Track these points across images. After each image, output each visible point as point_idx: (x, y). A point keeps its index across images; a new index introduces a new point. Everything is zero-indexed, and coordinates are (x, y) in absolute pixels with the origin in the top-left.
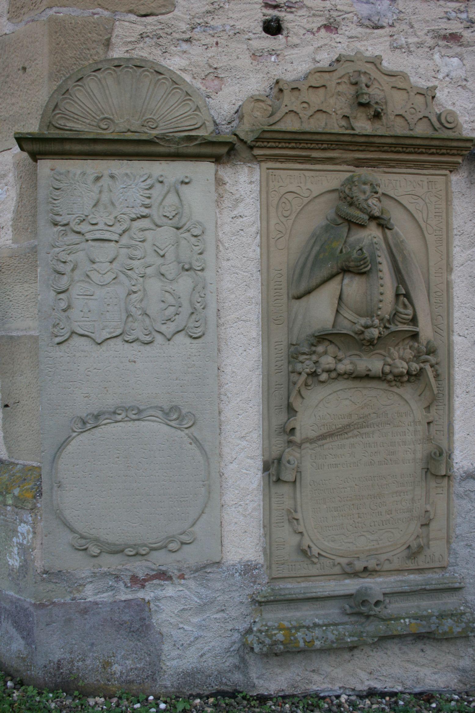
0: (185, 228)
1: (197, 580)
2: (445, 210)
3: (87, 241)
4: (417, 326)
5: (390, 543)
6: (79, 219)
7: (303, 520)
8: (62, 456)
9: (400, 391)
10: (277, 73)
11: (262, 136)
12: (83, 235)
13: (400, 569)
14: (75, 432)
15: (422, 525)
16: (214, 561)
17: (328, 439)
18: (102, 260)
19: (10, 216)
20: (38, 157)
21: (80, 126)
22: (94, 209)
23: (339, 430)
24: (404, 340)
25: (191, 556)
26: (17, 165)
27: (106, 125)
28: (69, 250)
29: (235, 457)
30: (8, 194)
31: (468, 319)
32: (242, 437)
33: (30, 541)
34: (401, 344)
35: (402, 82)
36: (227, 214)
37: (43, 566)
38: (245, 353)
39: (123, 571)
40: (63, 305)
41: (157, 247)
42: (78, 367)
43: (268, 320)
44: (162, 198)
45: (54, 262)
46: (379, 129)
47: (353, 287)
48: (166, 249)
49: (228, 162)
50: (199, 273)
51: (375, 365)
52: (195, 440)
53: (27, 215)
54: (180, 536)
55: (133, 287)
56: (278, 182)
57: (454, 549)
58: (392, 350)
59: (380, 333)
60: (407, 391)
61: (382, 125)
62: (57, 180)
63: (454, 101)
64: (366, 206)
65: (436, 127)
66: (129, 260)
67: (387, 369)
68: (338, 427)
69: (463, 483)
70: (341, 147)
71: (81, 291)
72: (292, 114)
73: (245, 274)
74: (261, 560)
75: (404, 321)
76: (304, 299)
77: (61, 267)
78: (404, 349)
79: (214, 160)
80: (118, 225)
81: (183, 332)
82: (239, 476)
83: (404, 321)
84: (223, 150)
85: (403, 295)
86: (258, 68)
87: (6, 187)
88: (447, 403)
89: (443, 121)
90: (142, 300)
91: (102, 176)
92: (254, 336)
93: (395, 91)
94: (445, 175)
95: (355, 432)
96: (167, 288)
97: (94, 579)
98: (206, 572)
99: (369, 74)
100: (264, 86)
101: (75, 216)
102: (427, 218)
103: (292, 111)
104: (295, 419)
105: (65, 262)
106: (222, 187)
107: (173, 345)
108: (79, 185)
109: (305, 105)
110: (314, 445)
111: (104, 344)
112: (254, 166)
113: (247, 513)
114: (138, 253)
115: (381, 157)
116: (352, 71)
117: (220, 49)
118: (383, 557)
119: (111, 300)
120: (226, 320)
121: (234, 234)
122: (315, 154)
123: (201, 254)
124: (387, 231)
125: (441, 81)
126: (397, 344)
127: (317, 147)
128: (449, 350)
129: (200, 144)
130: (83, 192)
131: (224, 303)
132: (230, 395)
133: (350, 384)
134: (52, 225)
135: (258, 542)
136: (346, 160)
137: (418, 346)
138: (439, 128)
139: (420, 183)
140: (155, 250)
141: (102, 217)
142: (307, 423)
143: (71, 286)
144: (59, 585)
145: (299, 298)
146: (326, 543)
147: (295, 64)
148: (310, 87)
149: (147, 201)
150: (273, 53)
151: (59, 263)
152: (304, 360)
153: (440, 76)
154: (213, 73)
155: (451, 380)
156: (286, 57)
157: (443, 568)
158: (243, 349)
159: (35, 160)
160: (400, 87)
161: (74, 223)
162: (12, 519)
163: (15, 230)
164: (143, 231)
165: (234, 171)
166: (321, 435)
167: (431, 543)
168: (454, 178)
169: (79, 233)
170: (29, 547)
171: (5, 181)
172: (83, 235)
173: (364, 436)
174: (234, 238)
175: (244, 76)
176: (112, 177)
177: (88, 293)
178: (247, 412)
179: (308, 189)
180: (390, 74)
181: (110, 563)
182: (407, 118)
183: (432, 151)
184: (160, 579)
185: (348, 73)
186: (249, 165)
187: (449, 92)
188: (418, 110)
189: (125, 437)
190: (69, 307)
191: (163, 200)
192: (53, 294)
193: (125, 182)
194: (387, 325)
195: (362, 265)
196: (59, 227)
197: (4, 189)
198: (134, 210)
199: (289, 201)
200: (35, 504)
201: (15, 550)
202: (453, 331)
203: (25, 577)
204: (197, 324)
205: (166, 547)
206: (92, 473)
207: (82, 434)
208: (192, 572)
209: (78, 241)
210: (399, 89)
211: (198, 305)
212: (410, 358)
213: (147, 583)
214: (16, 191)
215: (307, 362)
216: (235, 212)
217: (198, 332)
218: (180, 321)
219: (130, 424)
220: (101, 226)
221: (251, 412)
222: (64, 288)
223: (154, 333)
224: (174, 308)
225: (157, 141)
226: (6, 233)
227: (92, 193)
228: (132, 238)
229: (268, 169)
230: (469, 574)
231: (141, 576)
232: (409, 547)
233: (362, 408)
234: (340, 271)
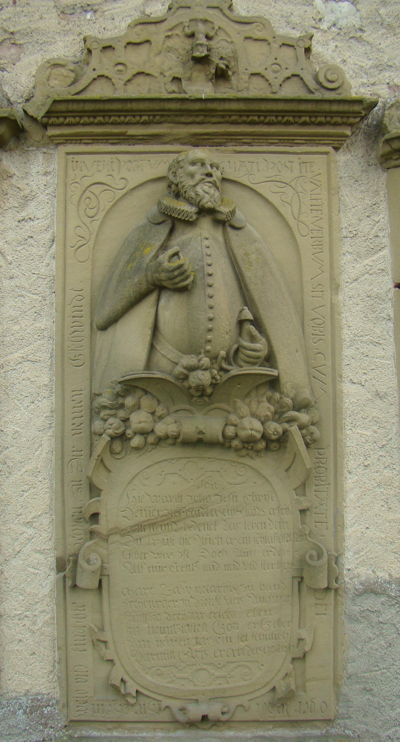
2: (326, 203)
4: (276, 368)
5: (245, 683)
7: (114, 642)
9: (257, 463)
10: (90, 31)
11: (53, 109)
13: (261, 719)
15: (294, 659)
17: (147, 531)
23: (164, 518)
24: (257, 387)
29: (18, 549)
31: (366, 358)
32: (28, 523)
34: (253, 394)
35: (260, 31)
38: (32, 406)
43: (63, 359)
46: (224, 91)
47: (171, 310)
49: (16, 148)
51: (211, 425)
56: (81, 170)
57: (345, 695)
58: (239, 403)
59: (213, 378)
60: (266, 464)
61: (230, 88)
63: (345, 58)
64: (193, 194)
65: (311, 89)
67: (230, 431)
68: (161, 513)
69: (359, 600)
70: (169, 119)
72: (103, 80)
73: (35, 297)
74: (57, 693)
75: (252, 360)
76: (110, 330)
78: (259, 402)
82: (25, 577)
83: (252, 360)
85: (252, 323)
86: (67, 28)
88: (332, 482)
89: (322, 79)
92: (45, 383)
93: (250, 44)
94: (327, 153)
95: (189, 522)
99: (212, 23)
100: (73, 50)
102: (299, 214)
103: (102, 76)
104: (99, 501)
106: (7, 181)
109: (120, 67)
110: (128, 538)
112: (51, 152)
113: (37, 628)
115: (228, 130)
116: (188, 20)
117: (18, 9)
118: (233, 703)
121: (20, 243)
122: (132, 131)
124: (231, 233)
125: (325, 32)
126: (248, 395)
127: (134, 120)
128: (335, 404)
131: (5, 336)
132: (11, 464)
133: (178, 452)
135: (52, 669)
136: (177, 137)
137: (281, 398)
138: (316, 90)
139: (289, 165)
142: (117, 506)
145: (104, 328)
146: (149, 677)
147: (117, 19)
148: (129, 44)
150: (89, 8)
152: (106, 417)
153: (324, 26)
154: (10, 39)
155: (339, 448)
156: (106, 13)
157: (328, 721)
160: (257, 37)
166: (138, 525)
167: (308, 684)
168: (342, 158)
173: (202, 528)
174: (20, 248)
175: (48, 40)
178: (35, 488)
179: (123, 178)
180: (242, 20)
182: (268, 78)
183: (303, 119)
185: (182, 23)
186: (45, 150)
187: (336, 46)
188: (284, 67)
194: (225, 366)
195: (176, 277)
199: (95, 195)
202: (341, 376)
210: (256, 40)
212: (266, 416)
215: (111, 420)
216: (24, 214)
221: (40, 488)
229: (68, 154)
230: (367, 731)
232: (274, 689)
233: (198, 487)
234: (152, 287)
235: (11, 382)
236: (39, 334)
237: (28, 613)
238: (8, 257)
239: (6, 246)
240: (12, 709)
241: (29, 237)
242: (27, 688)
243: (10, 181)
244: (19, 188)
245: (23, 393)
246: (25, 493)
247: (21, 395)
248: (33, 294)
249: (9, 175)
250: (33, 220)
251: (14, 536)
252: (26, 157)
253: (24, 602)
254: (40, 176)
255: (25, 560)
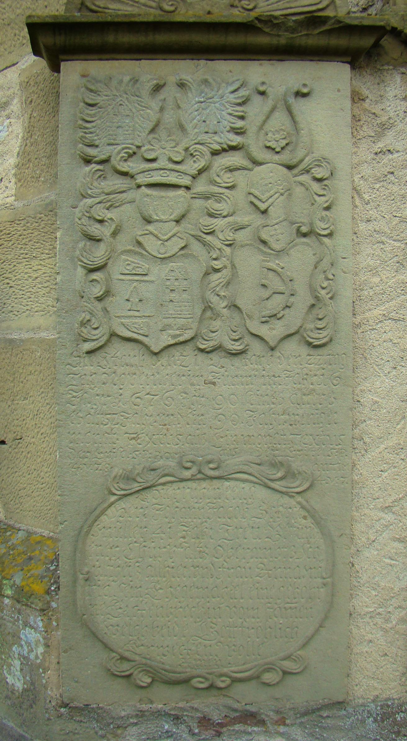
0: (301, 167)
1: (306, 727)
3: (139, 186)
6: (125, 153)
8: (92, 532)
12: (132, 177)
14: (115, 494)
16: (335, 699)
18: (163, 217)
19: (12, 161)
20: (61, 57)
21: (130, 9)
22: (152, 136)
25: (299, 692)
26: (25, 85)
27: (172, 5)
28: (109, 201)
29: (373, 538)
30: (10, 130)
32: (386, 507)
33: (41, 657)
36: (367, 147)
37: (61, 696)
38: (394, 372)
39: (188, 711)
40: (98, 291)
41: (256, 197)
42: (121, 391)
44: (264, 118)
45: (85, 221)
48: (271, 200)
49: (367, 66)
50: (326, 240)
52: (311, 513)
53: (38, 159)
54: (282, 662)
55: (215, 262)
62: (91, 91)
66: (207, 217)
71: (128, 267)
73: (396, 244)
77: (95, 230)
79: (349, 59)
80: (190, 161)
81: (296, 338)
84: (367, 42)
87: (8, 121)
90: (228, 283)
91: (165, 84)
96: (272, 265)
97: (140, 719)
98: (321, 716)
101: (119, 148)
105: (101, 222)
107: (279, 357)
108: (127, 98)
111: (163, 354)
113: (390, 625)
114: (223, 207)
119: (176, 283)
120: (365, 318)
121: (378, 180)
123: (328, 208)
129: (330, 32)
130: (134, 110)
131: (362, 290)
132: (367, 440)
134: (82, 162)
140: (252, 203)
141: (164, 149)
143: (111, 260)
144: (85, 725)
149: (240, 124)
151: (92, 222)
158: (391, 364)
159: (55, 68)
161: (118, 158)
162: (11, 617)
163: (20, 181)
164: (231, 171)
165: (377, 80)
169: (125, 174)
170: (39, 666)
171: (6, 112)
172: (132, 177)
176: (182, 85)
177: (140, 271)
178: (395, 467)
181: (166, 699)
184: (245, 723)
189: (196, 505)
190: (107, 293)
191: (265, 122)
192: (80, 271)
193: (202, 92)
196: (93, 165)
197: (5, 124)
198: (216, 138)
200: (48, 603)
201: (17, 663)
203: (31, 706)
204: (320, 324)
205: (258, 677)
206: (140, 559)
207: (125, 499)
208: (298, 715)
209: (124, 187)
211: (323, 292)
213: (225, 729)
214: (23, 125)
216: (380, 145)
217: (322, 337)
218: (294, 319)
219: (204, 484)
220: (162, 163)
222: (99, 262)
223: (248, 339)
224: (281, 296)
225: (259, 25)
226: (7, 187)
227: (149, 111)
228: (213, 183)
231: (216, 717)
235: (369, 344)
236: (402, 288)
237: (381, 610)
238: (364, 195)
239: (361, 182)
240: (360, 717)
241: (388, 172)
242: (376, 693)
243: (361, 105)
244: (374, 114)
245: (383, 357)
246: (383, 473)
247: (382, 359)
248: (394, 240)
249: (361, 98)
250: (392, 153)
251: (369, 523)
252: (380, 77)
253: (377, 597)
254: (398, 101)
255: (381, 549)
